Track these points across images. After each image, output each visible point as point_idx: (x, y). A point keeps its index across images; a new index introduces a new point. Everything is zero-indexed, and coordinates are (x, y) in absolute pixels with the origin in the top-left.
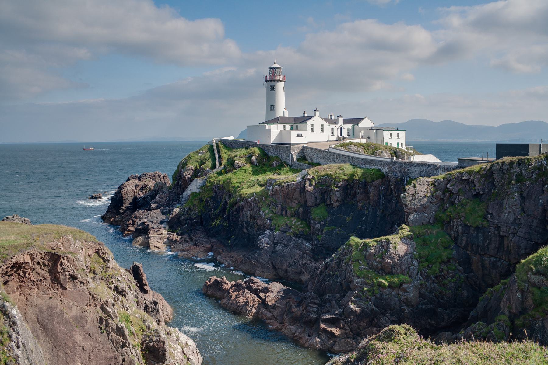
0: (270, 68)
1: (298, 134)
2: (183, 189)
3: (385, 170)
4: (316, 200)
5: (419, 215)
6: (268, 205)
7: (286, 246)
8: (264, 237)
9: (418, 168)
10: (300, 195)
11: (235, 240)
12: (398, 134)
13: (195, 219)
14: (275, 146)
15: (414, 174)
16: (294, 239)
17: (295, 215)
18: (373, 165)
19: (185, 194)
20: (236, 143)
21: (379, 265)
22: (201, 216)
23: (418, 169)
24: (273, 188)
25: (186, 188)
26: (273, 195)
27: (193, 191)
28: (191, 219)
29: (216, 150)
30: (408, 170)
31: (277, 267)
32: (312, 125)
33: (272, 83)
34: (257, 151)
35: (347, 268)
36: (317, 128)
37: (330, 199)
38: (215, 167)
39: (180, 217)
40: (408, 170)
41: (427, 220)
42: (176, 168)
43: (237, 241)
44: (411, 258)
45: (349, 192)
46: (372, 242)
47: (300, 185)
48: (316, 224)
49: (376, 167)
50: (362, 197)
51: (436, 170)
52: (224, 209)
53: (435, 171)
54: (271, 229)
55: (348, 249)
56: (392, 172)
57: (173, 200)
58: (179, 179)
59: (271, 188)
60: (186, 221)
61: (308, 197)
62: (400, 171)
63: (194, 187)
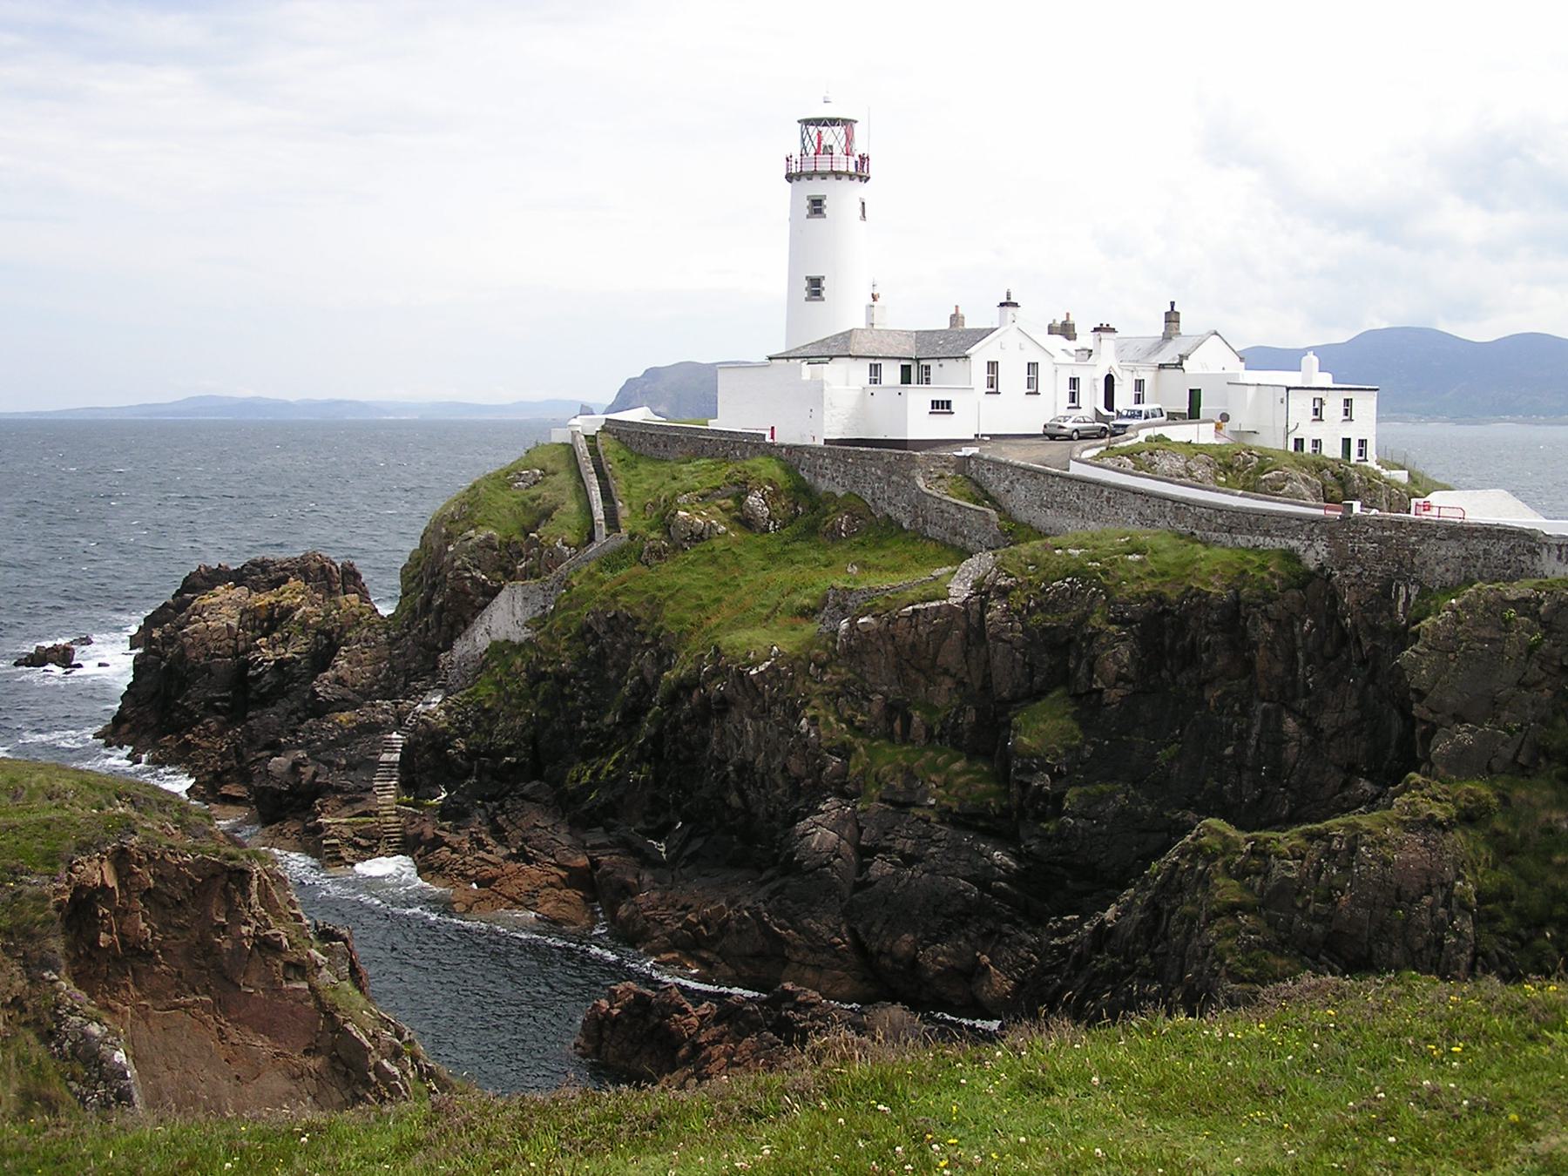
0: (807, 122)
1: (936, 404)
2: (452, 627)
3: (1315, 554)
4: (1031, 676)
5: (1470, 731)
6: (832, 697)
7: (909, 860)
8: (817, 824)
9: (1453, 543)
10: (966, 654)
11: (690, 837)
12: (1348, 402)
13: (509, 751)
14: (846, 454)
15: (1439, 569)
16: (943, 831)
17: (947, 736)
18: (1267, 533)
19: (461, 647)
20: (676, 439)
21: (1318, 928)
22: (534, 741)
23: (1452, 549)
24: (852, 624)
25: (467, 624)
26: (850, 652)
27: (500, 636)
28: (496, 755)
29: (588, 468)
30: (1413, 552)
31: (875, 947)
32: (993, 366)
33: (816, 188)
34: (770, 469)
35: (1188, 939)
36: (1012, 378)
37: (1091, 670)
38: (591, 539)
39: (447, 744)
40: (1413, 552)
41: (1507, 753)
42: (417, 544)
43: (697, 844)
44: (1446, 903)
45: (1167, 642)
46: (1286, 840)
47: (966, 612)
48: (1032, 772)
49: (1278, 543)
50: (1220, 662)
51: (1533, 552)
52: (633, 714)
53: (1527, 558)
54: (842, 794)
55: (1193, 868)
56: (1344, 559)
57: (411, 676)
58: (433, 587)
59: (844, 624)
60: (469, 759)
61: (997, 660)
62: (1379, 560)
63: (506, 618)
